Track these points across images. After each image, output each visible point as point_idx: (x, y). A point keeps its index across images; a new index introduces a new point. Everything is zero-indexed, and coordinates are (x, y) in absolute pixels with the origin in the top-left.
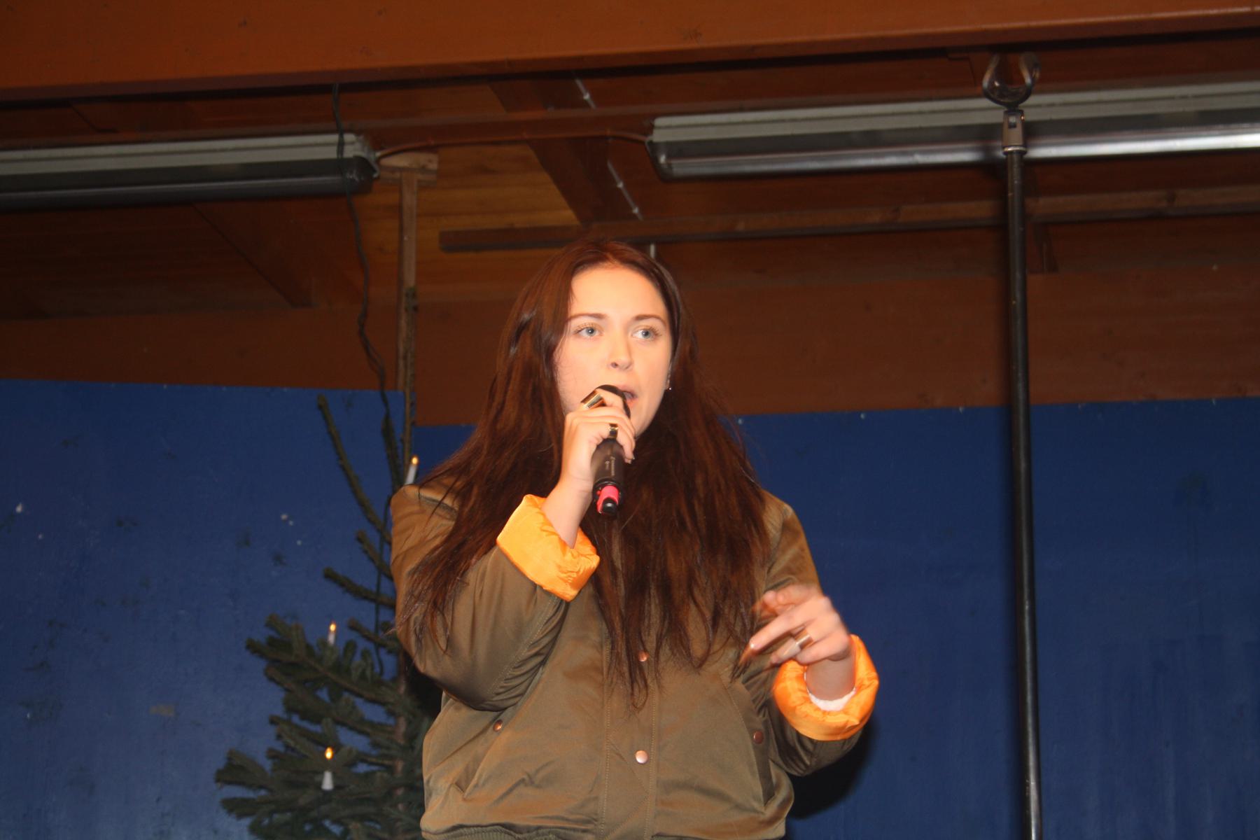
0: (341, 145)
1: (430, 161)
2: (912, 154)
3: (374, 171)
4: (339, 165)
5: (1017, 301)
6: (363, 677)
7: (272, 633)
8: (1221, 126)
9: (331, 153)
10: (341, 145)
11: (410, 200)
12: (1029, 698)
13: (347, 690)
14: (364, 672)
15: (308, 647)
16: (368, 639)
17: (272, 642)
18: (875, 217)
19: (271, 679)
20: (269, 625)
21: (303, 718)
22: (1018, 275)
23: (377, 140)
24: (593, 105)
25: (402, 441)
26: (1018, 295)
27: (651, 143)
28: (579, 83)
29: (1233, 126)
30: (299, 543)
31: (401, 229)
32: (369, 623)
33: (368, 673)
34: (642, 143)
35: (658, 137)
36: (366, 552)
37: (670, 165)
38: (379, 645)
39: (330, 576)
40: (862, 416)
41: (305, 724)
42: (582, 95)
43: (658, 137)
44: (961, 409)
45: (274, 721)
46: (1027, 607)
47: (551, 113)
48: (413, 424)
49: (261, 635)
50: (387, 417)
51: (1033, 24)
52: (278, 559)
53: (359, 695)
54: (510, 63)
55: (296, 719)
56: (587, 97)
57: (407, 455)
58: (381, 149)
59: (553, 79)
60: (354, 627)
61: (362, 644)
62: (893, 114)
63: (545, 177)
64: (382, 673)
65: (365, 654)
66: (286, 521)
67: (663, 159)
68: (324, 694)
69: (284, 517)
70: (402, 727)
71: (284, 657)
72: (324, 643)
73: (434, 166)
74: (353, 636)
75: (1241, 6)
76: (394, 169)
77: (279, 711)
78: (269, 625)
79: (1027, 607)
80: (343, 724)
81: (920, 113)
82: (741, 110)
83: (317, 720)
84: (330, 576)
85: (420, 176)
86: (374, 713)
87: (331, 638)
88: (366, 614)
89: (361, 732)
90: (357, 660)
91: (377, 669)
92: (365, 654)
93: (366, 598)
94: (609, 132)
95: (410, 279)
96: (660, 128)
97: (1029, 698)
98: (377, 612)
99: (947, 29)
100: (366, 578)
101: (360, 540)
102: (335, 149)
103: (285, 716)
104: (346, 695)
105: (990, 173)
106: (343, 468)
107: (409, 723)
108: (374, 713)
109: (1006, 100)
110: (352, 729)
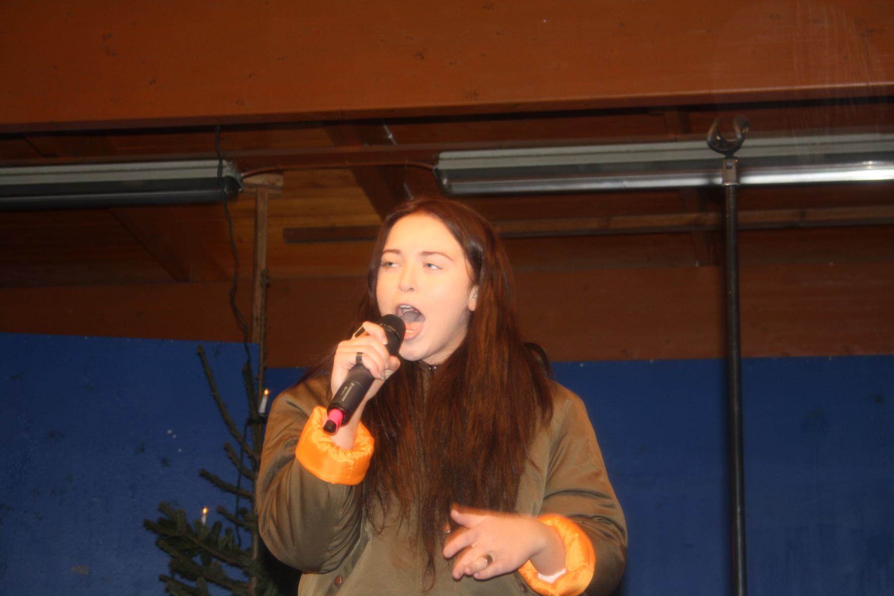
0: (220, 168)
1: (278, 180)
2: (621, 180)
3: (240, 187)
4: (218, 182)
5: (732, 292)
6: (226, 547)
7: (163, 516)
8: (839, 165)
9: (213, 174)
10: (220, 168)
11: (262, 207)
12: (740, 575)
13: (215, 557)
14: (227, 545)
15: (188, 526)
16: (231, 520)
17: (162, 522)
18: (592, 224)
19: (162, 549)
20: (161, 509)
21: (183, 576)
22: (733, 273)
23: (243, 165)
24: (394, 142)
25: (257, 379)
26: (733, 287)
27: (437, 170)
28: (386, 127)
29: (836, 165)
30: (180, 450)
31: (256, 228)
32: (231, 510)
33: (230, 545)
34: (430, 170)
35: (441, 166)
36: (230, 458)
37: (450, 186)
38: (239, 525)
39: (204, 475)
40: (581, 365)
41: (185, 581)
42: (387, 135)
43: (441, 166)
44: (651, 361)
45: (162, 579)
46: (739, 510)
47: (366, 148)
48: (265, 368)
49: (154, 516)
50: (249, 362)
51: (871, 84)
52: (164, 462)
53: (224, 561)
54: (342, 113)
55: (177, 577)
56: (391, 136)
57: (260, 388)
58: (244, 171)
59: (368, 124)
60: (221, 511)
61: (226, 524)
62: (609, 153)
63: (359, 191)
64: (240, 545)
65: (228, 531)
66: (171, 435)
67: (445, 182)
68: (198, 560)
69: (170, 432)
70: (254, 584)
71: (171, 533)
72: (199, 523)
73: (280, 184)
74: (220, 518)
75: (860, 82)
76: (252, 186)
77: (166, 571)
78: (161, 509)
79: (739, 510)
80: (212, 582)
81: (628, 152)
82: (500, 148)
83: (193, 578)
84: (204, 475)
85: (271, 191)
86: (235, 574)
87: (204, 520)
88: (230, 503)
89: (225, 587)
90: (222, 535)
91: (237, 542)
92: (228, 531)
93: (229, 491)
94: (407, 162)
95: (262, 264)
96: (443, 159)
97: (740, 575)
98: (238, 501)
99: (653, 94)
100: (230, 476)
101: (226, 449)
102: (216, 170)
103: (170, 576)
104: (214, 560)
105: (711, 196)
106: (215, 397)
107: (259, 581)
108: (235, 574)
109: (725, 150)
110: (218, 585)
